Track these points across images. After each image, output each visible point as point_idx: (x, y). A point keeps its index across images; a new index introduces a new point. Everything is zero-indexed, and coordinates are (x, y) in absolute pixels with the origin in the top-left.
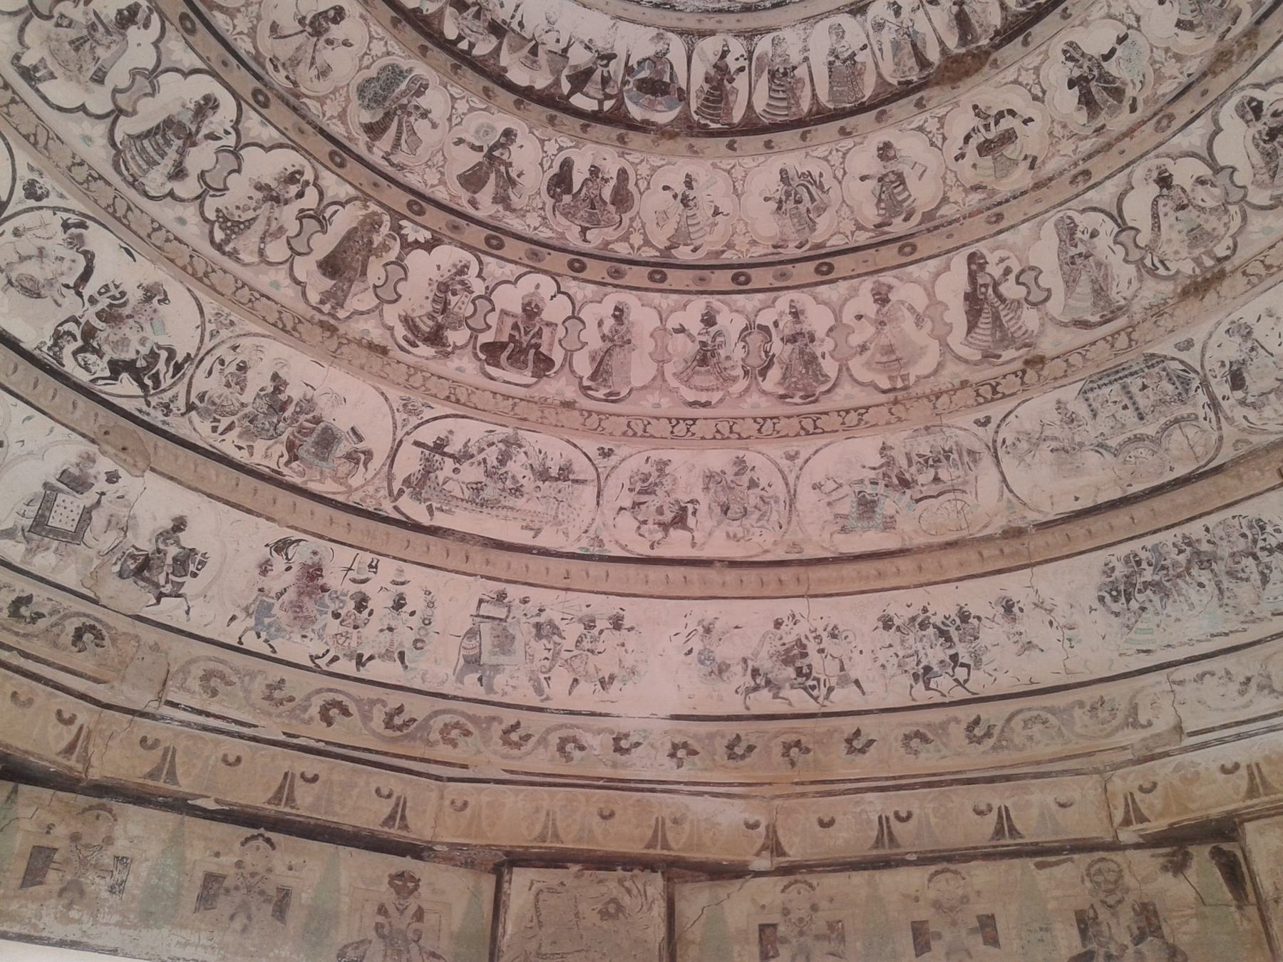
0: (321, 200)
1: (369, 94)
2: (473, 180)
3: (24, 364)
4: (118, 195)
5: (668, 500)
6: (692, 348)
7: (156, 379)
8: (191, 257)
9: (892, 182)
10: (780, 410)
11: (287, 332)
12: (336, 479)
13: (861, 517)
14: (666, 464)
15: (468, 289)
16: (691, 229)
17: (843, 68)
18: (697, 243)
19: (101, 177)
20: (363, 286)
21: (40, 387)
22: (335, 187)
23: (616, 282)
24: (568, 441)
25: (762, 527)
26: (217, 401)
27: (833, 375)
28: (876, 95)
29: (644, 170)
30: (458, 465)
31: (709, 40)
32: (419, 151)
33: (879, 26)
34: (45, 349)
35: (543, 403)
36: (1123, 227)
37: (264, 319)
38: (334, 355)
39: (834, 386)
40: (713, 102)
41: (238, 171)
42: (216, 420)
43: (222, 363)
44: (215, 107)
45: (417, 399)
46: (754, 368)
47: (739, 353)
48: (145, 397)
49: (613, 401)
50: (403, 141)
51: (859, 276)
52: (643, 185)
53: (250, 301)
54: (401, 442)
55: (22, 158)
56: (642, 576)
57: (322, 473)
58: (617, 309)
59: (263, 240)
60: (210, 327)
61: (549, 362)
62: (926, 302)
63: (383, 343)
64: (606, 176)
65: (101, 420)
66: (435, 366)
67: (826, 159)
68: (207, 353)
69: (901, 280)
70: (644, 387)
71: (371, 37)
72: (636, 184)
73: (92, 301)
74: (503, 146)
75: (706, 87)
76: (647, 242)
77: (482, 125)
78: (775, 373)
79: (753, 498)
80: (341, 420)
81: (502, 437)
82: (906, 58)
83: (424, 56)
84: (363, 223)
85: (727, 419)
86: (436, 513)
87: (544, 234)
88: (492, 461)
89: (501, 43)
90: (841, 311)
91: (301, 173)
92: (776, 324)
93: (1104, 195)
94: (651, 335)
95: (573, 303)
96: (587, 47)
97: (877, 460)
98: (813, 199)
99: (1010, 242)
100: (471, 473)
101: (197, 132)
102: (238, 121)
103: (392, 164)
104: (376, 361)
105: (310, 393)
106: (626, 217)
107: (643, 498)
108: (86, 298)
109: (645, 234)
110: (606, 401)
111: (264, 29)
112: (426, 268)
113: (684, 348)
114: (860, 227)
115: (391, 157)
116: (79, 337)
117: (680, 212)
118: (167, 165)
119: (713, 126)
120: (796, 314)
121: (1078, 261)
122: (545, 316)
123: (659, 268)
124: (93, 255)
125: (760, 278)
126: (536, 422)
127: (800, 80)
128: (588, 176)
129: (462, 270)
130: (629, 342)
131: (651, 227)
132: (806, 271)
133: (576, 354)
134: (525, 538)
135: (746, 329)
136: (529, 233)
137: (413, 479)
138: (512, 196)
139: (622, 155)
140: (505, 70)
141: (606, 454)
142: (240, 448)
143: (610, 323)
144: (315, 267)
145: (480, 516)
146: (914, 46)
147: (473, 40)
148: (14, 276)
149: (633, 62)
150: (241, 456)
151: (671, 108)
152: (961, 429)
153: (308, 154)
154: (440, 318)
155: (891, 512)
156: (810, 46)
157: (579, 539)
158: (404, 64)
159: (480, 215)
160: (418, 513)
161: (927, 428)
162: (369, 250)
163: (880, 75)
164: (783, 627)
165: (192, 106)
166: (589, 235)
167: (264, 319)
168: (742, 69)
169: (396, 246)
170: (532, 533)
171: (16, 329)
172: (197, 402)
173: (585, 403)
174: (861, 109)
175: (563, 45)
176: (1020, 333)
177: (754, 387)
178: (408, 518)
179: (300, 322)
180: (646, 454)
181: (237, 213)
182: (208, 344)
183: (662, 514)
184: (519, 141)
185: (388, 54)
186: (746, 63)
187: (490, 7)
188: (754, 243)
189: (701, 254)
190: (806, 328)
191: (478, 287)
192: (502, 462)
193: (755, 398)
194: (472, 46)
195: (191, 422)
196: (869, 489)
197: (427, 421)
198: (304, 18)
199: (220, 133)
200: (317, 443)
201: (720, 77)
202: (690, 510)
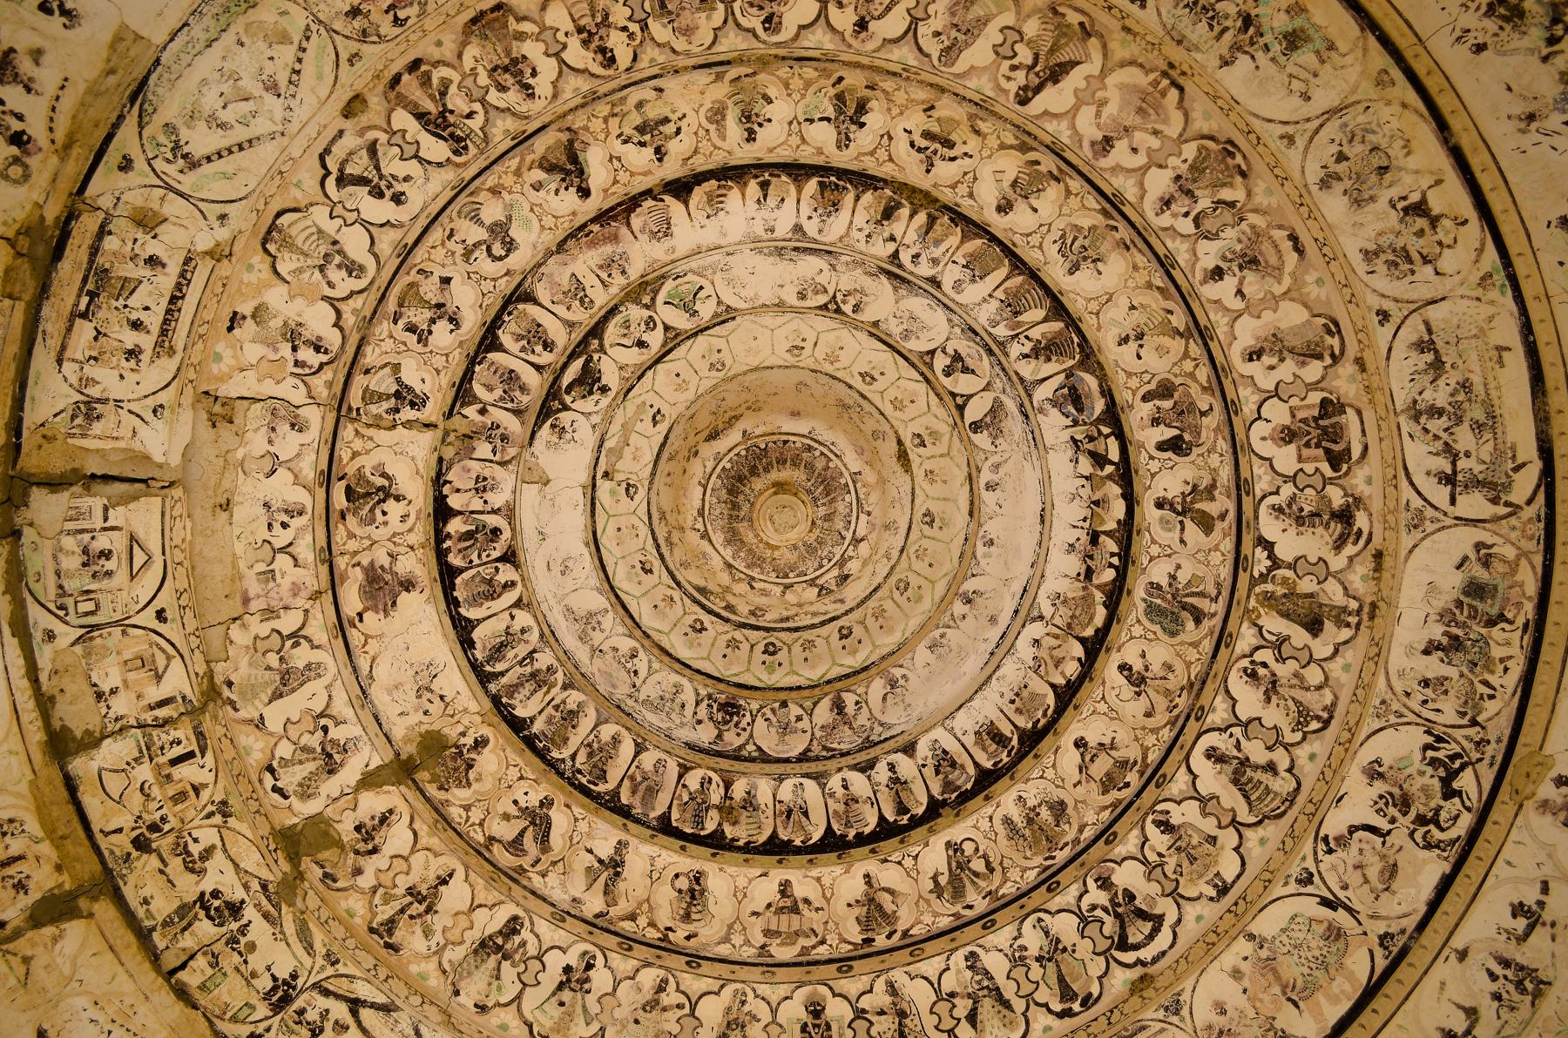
1: (1173, 627)
2: (1206, 523)
3: (1466, 870)
5: (1404, 232)
6: (1250, 276)
13: (1308, 39)
15: (1293, 499)
22: (1246, 638)
24: (1388, 358)
27: (1194, 145)
28: (977, 236)
29: (1134, 382)
31: (1022, 373)
33: (935, 261)
36: (915, 21)
39: (1203, 137)
41: (1259, 719)
42: (1482, 697)
43: (1425, 702)
44: (1214, 749)
45: (1404, 517)
47: (1230, 233)
49: (1337, 324)
52: (1147, 377)
55: (1279, 891)
58: (1251, 360)
59: (1308, 689)
60: (1393, 719)
61: (1325, 403)
62: (1084, 108)
63: (1370, 558)
65: (1506, 798)
67: (1040, 247)
69: (1080, 141)
70: (1306, 306)
73: (1393, 821)
74: (1172, 505)
75: (1054, 358)
76: (1186, 355)
78: (1226, 194)
79: (1355, 150)
80: (1452, 583)
81: (1412, 423)
84: (1270, 607)
86: (1519, 461)
87: (1223, 445)
88: (1443, 422)
90: (1140, 168)
91: (1245, 670)
92: (1186, 215)
93: (905, 54)
97: (1243, 61)
98: (1075, 239)
99: (991, 85)
100: (1464, 438)
102: (1219, 729)
104: (1388, 562)
105: (1433, 617)
106: (1178, 381)
107: (1416, 257)
110: (1339, 332)
111: (1152, 723)
112: (1289, 543)
113: (1254, 284)
114: (1068, 192)
118: (1265, 778)
119: (1076, 340)
120: (1167, 203)
121: (964, 29)
122: (1287, 421)
127: (1005, 291)
128: (1162, 426)
129: (1279, 510)
130: (1274, 335)
134: (1517, 363)
136: (1229, 458)
137: (1490, 496)
140: (1119, 522)
141: (1384, 316)
142: (1506, 669)
143: (1267, 360)
145: (1506, 415)
146: (927, 233)
148: (1381, 887)
150: (1517, 669)
152: (1159, 14)
153: (1228, 669)
155: (1283, 16)
157: (1492, 302)
158: (1141, 606)
159: (1231, 506)
160: (1526, 482)
161: (1179, 42)
162: (1291, 595)
164: (1480, 41)
166: (1205, 407)
169: (1281, 573)
170: (1505, 354)
173: (1352, 350)
175: (1083, 481)
176: (1050, 27)
177: (1249, 207)
178: (1538, 486)
182: (1411, 717)
183: (1422, 231)
188: (1135, 268)
189: (1170, 305)
190: (1173, 188)
191: (1287, 490)
192: (1441, 412)
193: (1260, 199)
194: (1113, 554)
196: (1276, 48)
197: (1425, 500)
199: (1233, 740)
200: (1482, 599)
201: (1042, 351)
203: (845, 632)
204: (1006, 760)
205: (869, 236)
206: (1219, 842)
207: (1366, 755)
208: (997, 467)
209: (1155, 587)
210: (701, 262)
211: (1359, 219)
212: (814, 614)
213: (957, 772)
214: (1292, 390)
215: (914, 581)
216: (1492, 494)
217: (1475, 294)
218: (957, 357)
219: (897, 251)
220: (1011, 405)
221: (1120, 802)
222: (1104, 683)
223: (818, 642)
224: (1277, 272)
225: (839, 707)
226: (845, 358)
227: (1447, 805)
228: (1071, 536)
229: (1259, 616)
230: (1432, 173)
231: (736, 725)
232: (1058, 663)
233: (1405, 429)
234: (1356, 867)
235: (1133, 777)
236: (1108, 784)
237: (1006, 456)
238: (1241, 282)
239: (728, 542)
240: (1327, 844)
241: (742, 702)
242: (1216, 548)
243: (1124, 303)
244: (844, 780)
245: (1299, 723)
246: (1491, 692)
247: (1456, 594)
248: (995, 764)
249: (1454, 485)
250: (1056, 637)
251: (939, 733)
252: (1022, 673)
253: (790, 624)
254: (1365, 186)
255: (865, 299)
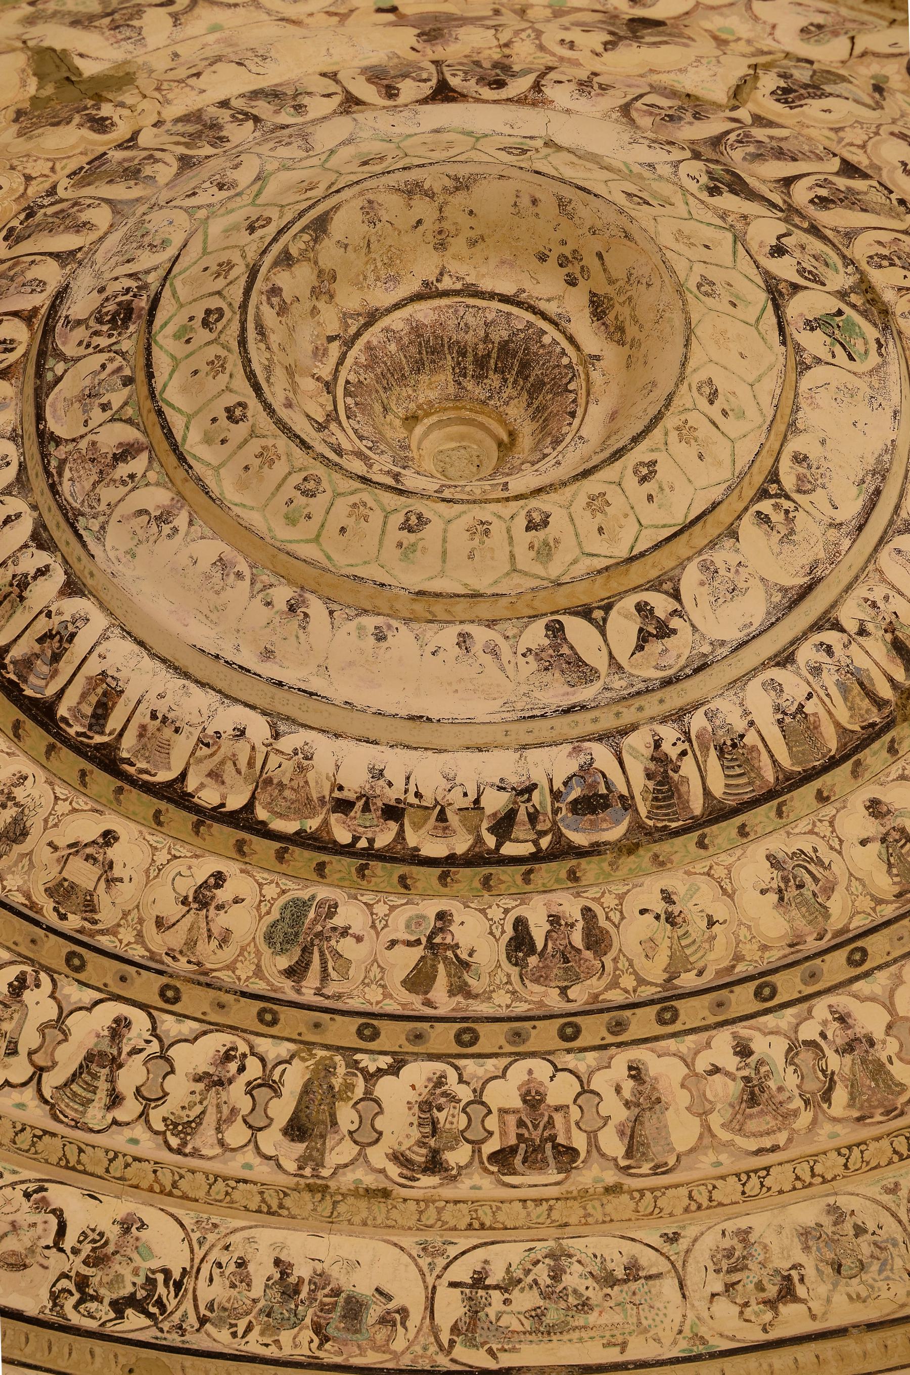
0: (264, 1066)
2: (420, 980)
4: (67, 1141)
5: (764, 1272)
6: (734, 1088)
7: (160, 1304)
8: (155, 1172)
9: (897, 841)
10: (864, 1133)
11: (273, 1214)
12: (377, 1349)
14: (748, 1231)
15: (454, 1099)
16: (688, 951)
17: (795, 723)
18: (700, 964)
19: (45, 1132)
20: (337, 1137)
21: (55, 1349)
23: (619, 1039)
24: (623, 1237)
25: (888, 1278)
26: (228, 1305)
29: (610, 901)
30: (507, 1295)
32: (351, 973)
33: (816, 670)
34: (47, 1311)
35: (584, 1194)
37: (246, 1208)
38: (331, 1220)
40: (664, 799)
41: (173, 1071)
42: (232, 1326)
43: (220, 1265)
44: (128, 1025)
45: (435, 1238)
46: (813, 1094)
47: (791, 1081)
48: (156, 1324)
49: (663, 1173)
50: (330, 970)
51: (895, 961)
53: (227, 1193)
54: (434, 1287)
56: (765, 1366)
57: (359, 1347)
58: (630, 1068)
59: (218, 1130)
60: (195, 1236)
61: (572, 1152)
63: (381, 1186)
64: (570, 921)
65: (122, 1360)
66: (449, 1192)
68: (202, 1261)
70: (692, 1150)
71: (260, 885)
72: (607, 918)
73: (75, 1251)
74: (441, 930)
75: (651, 785)
76: (641, 981)
77: (411, 918)
78: (840, 1095)
79: (865, 1247)
80: (361, 1284)
81: (545, 1251)
82: (858, 700)
83: (323, 876)
84: (315, 1071)
85: (805, 1158)
86: (499, 1355)
87: (521, 1008)
88: (544, 1279)
89: (402, 826)
90: (892, 1004)
91: (234, 1049)
92: (823, 1035)
94: (683, 1086)
95: (578, 1077)
96: (500, 788)
98: (815, 879)
100: (525, 1300)
101: (120, 1054)
102: (154, 1028)
103: (328, 997)
104: (379, 1209)
105: (319, 1267)
106: (608, 960)
107: (735, 1277)
108: (68, 1251)
109: (635, 973)
112: (399, 1093)
113: (724, 1090)
115: (324, 991)
116: (74, 1290)
117: (668, 933)
118: (102, 1097)
120: (842, 1019)
122: (551, 1100)
123: (667, 1005)
124: (61, 1211)
125: (789, 985)
126: (580, 1224)
127: (754, 748)
128: (548, 927)
129: (440, 1081)
130: (659, 1101)
131: (640, 963)
132: (836, 966)
133: (599, 1134)
135: (790, 1049)
136: (503, 1012)
137: (460, 1324)
138: (471, 981)
139: (578, 895)
140: (417, 849)
141: (673, 1239)
142: (267, 1345)
143: (628, 1085)
144: (280, 1136)
145: (550, 1345)
146: (861, 684)
147: (370, 835)
149: (558, 785)
150: (271, 1352)
151: (618, 822)
154: (432, 1142)
156: (750, 708)
158: (305, 895)
159: (441, 1012)
162: (333, 1096)
163: (837, 724)
165: (106, 1033)
166: (572, 993)
167: (246, 1208)
168: (684, 753)
169: (360, 1082)
170: (618, 1349)
171: (14, 1302)
172: (208, 1314)
173: (631, 1183)
174: (833, 763)
175: (472, 796)
177: (821, 1116)
179: (286, 1194)
180: (719, 1228)
181: (183, 1113)
182: (199, 1254)
184: (457, 919)
185: (284, 892)
186: (686, 745)
187: (378, 792)
190: (859, 1031)
191: (465, 1094)
192: (556, 1275)
193: (827, 1128)
194: (371, 841)
195: (208, 1335)
197: (456, 1258)
198: (186, 898)
199: (142, 1045)
200: (344, 1317)
201: (662, 771)
202: (796, 1278)
203: (238, 412)
204: (72, 731)
205: (874, 605)
206: (12, 1060)
207: (148, 1214)
208: (494, 652)
209: (332, 909)
210: (894, 377)
211: (787, 1231)
212: (268, 369)
213: (45, 669)
214: (590, 1113)
215: (317, 505)
216: (463, 1326)
217: (687, 1332)
218: (664, 631)
219: (843, 630)
220: (586, 693)
221: (39, 911)
222: (197, 856)
223: (223, 378)
224: (737, 1126)
225: (126, 453)
226: (684, 452)
227: (105, 1307)
228: (395, 774)
229: (303, 1060)
230: (825, 1313)
231: (96, 333)
232: (215, 775)
233: (539, 1245)
234: (13, 1224)
235: (74, 922)
236: (62, 891)
237: (510, 669)
238: (728, 1074)
239: (417, 329)
240: (36, 1192)
241: (132, 328)
242: (386, 995)
243: (720, 911)
244: (18, 516)
245: (176, 1125)
246: (240, 1334)
247: (347, 1287)
248: (64, 720)
249: (472, 1286)
250: (251, 764)
251: (99, 621)
252: (196, 719)
253: (251, 334)
254: (822, 1245)
255: (776, 537)
